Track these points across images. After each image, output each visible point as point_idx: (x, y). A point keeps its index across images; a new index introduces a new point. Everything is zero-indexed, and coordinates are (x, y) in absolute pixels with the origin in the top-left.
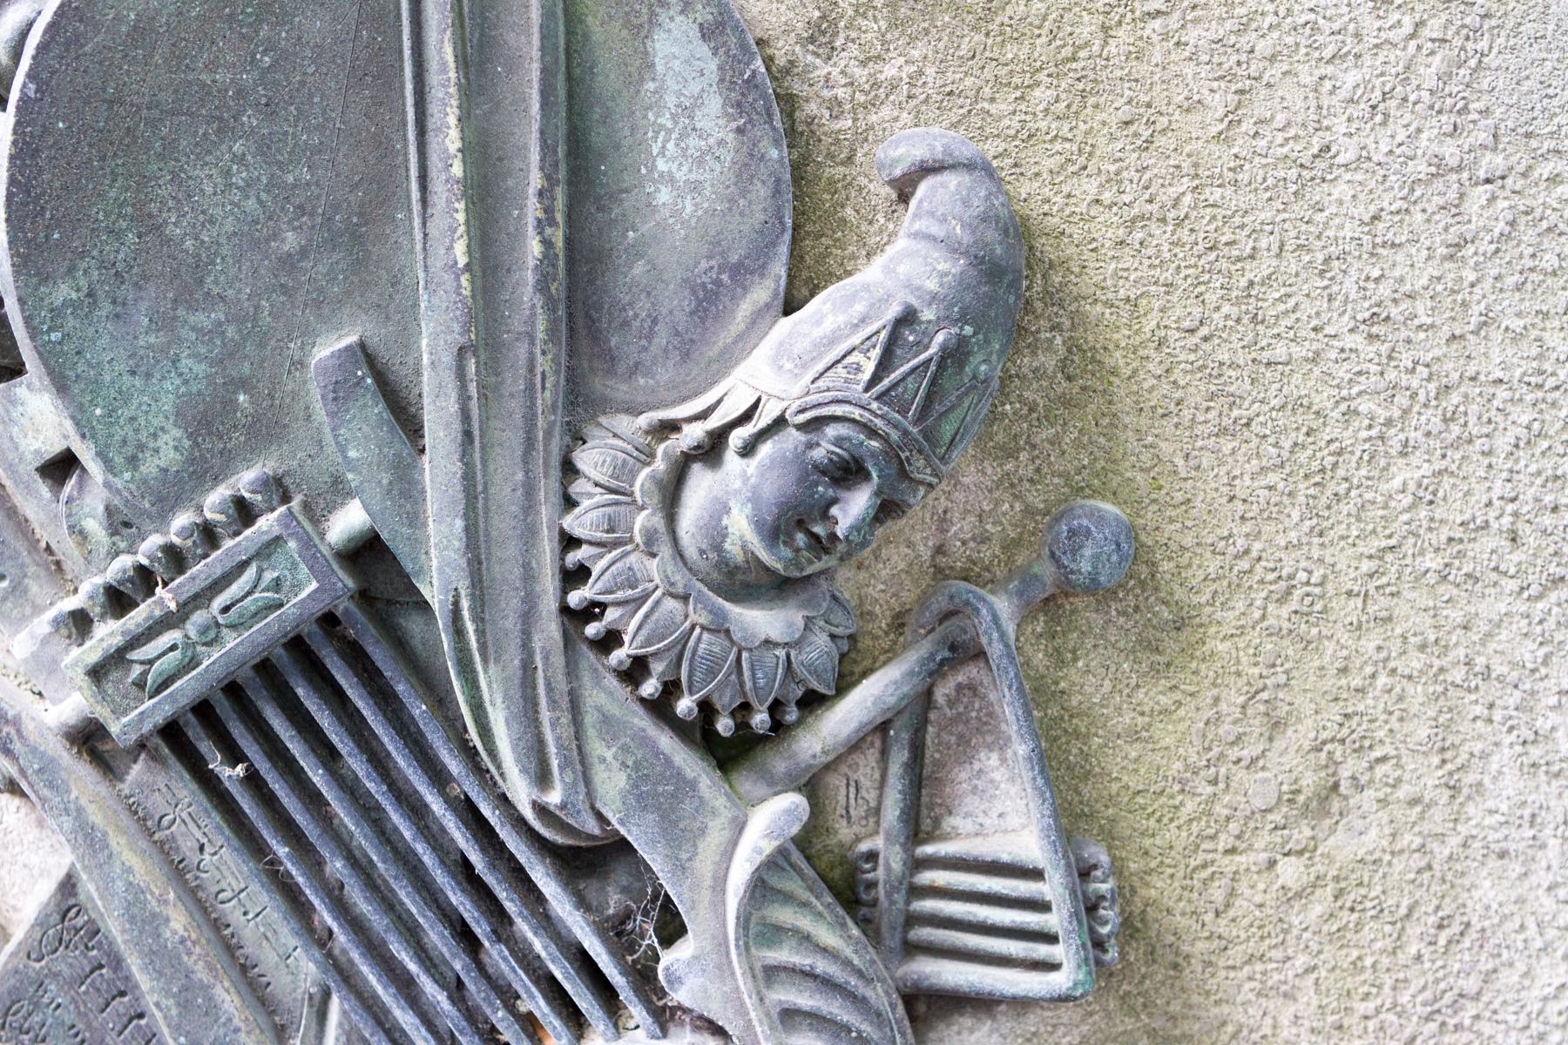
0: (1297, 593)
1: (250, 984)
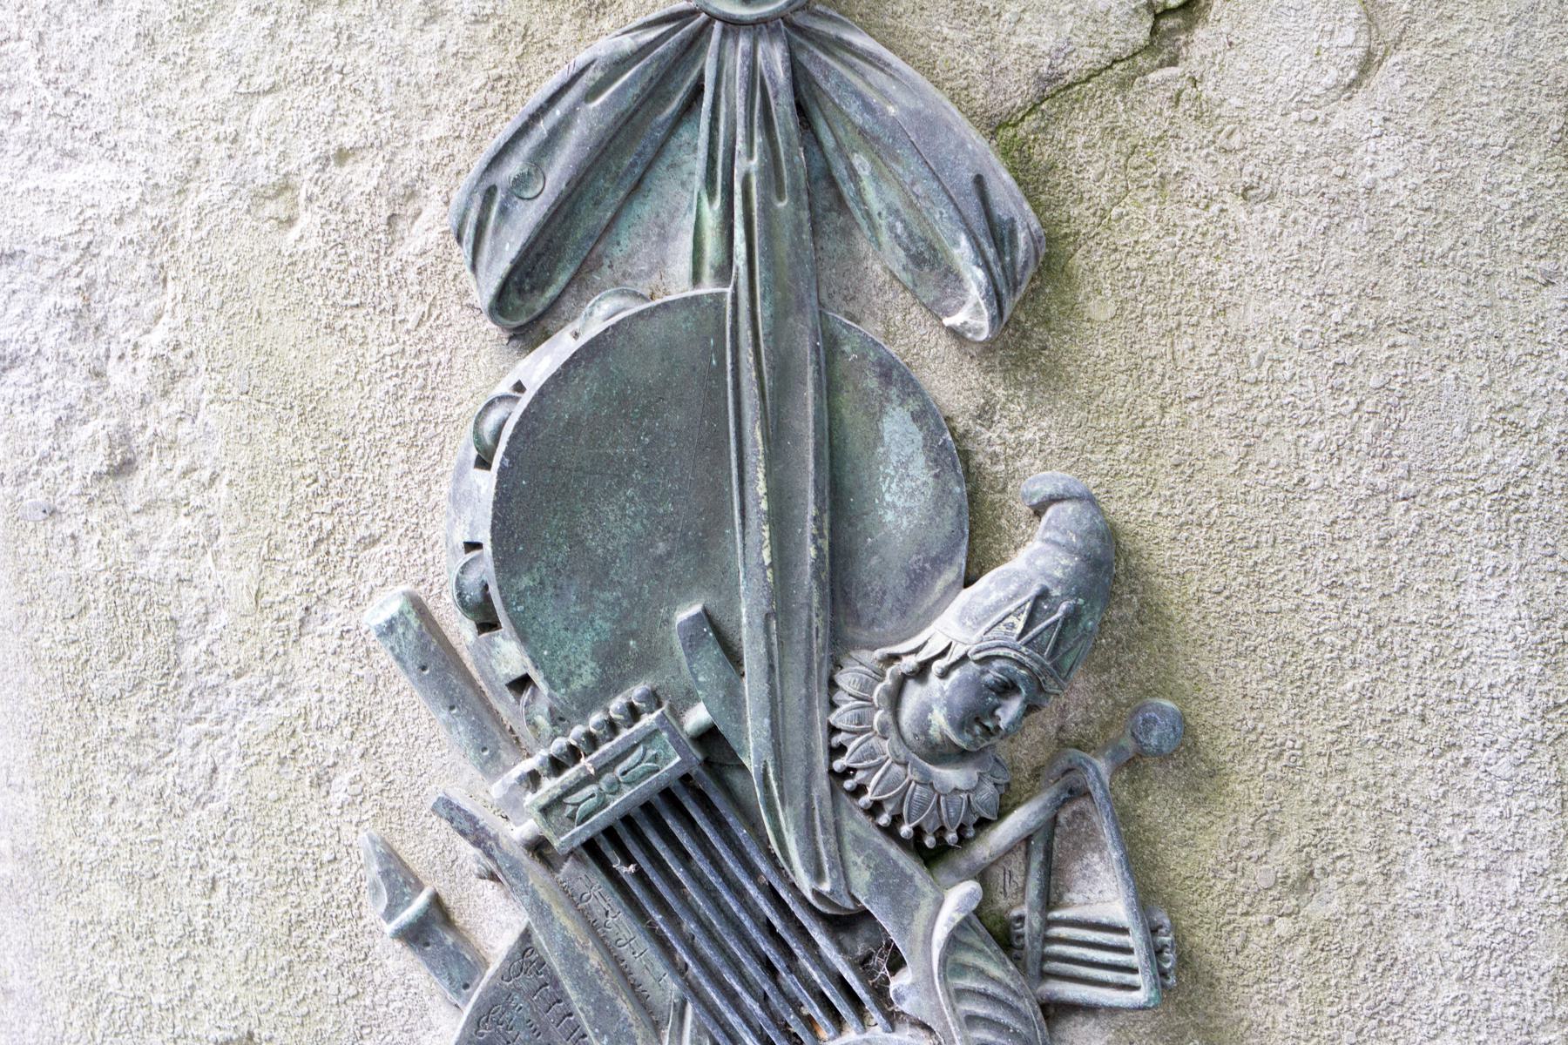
0: (1287, 754)
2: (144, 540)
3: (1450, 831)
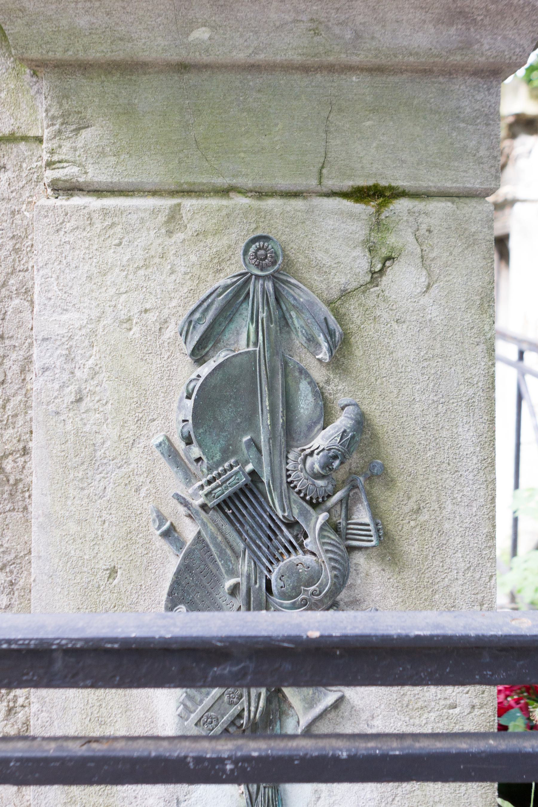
2: (85, 421)
3: (457, 495)
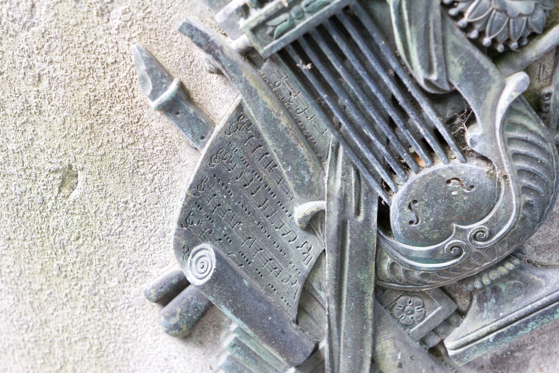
1: (309, 143)
